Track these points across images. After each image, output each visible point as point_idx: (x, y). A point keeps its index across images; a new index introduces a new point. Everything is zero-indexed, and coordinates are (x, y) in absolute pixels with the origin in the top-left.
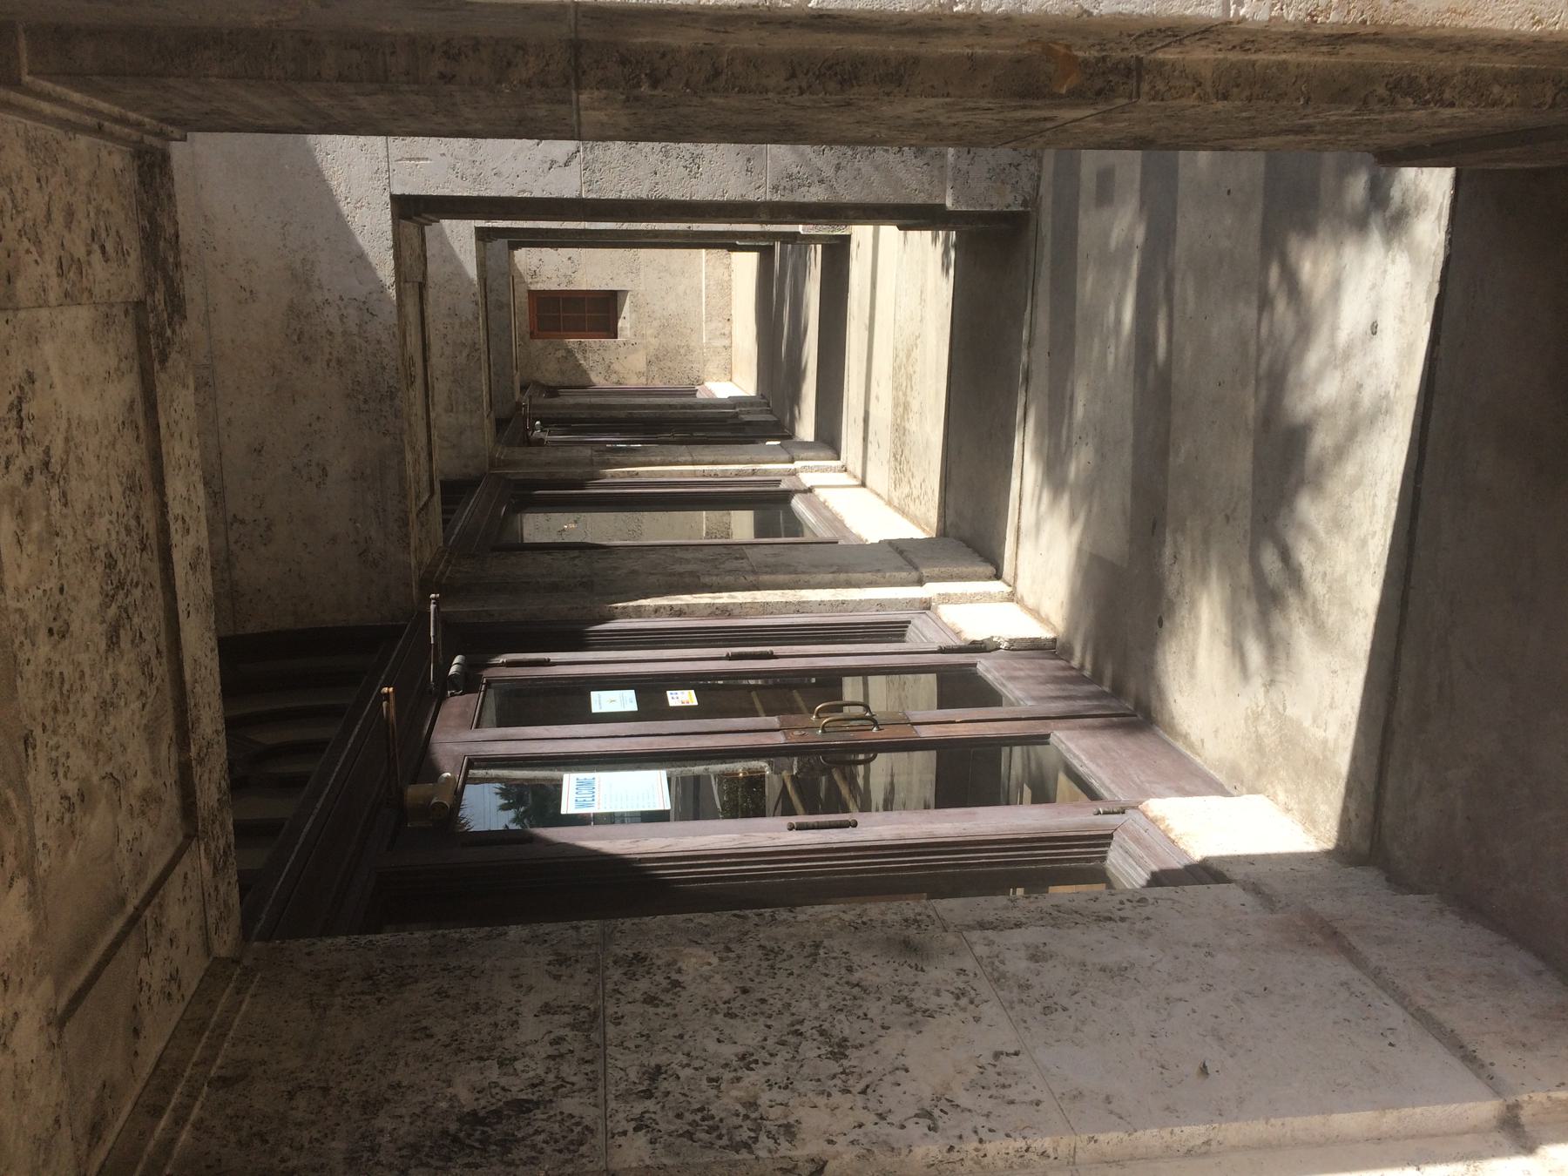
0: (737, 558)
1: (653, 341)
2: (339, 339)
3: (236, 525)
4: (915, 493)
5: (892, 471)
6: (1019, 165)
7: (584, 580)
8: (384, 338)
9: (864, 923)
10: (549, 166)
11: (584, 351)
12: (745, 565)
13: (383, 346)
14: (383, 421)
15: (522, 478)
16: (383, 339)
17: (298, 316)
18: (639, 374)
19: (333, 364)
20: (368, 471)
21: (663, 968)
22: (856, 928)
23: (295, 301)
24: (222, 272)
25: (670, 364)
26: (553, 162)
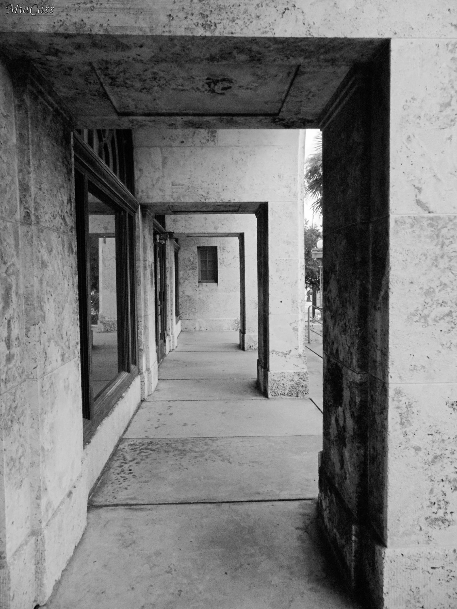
4: (126, 467)
5: (140, 441)
8: (263, 23)
10: (417, 186)
11: (193, 269)
12: (54, 364)
13: (254, 22)
18: (183, 292)
25: (188, 304)
26: (420, 190)
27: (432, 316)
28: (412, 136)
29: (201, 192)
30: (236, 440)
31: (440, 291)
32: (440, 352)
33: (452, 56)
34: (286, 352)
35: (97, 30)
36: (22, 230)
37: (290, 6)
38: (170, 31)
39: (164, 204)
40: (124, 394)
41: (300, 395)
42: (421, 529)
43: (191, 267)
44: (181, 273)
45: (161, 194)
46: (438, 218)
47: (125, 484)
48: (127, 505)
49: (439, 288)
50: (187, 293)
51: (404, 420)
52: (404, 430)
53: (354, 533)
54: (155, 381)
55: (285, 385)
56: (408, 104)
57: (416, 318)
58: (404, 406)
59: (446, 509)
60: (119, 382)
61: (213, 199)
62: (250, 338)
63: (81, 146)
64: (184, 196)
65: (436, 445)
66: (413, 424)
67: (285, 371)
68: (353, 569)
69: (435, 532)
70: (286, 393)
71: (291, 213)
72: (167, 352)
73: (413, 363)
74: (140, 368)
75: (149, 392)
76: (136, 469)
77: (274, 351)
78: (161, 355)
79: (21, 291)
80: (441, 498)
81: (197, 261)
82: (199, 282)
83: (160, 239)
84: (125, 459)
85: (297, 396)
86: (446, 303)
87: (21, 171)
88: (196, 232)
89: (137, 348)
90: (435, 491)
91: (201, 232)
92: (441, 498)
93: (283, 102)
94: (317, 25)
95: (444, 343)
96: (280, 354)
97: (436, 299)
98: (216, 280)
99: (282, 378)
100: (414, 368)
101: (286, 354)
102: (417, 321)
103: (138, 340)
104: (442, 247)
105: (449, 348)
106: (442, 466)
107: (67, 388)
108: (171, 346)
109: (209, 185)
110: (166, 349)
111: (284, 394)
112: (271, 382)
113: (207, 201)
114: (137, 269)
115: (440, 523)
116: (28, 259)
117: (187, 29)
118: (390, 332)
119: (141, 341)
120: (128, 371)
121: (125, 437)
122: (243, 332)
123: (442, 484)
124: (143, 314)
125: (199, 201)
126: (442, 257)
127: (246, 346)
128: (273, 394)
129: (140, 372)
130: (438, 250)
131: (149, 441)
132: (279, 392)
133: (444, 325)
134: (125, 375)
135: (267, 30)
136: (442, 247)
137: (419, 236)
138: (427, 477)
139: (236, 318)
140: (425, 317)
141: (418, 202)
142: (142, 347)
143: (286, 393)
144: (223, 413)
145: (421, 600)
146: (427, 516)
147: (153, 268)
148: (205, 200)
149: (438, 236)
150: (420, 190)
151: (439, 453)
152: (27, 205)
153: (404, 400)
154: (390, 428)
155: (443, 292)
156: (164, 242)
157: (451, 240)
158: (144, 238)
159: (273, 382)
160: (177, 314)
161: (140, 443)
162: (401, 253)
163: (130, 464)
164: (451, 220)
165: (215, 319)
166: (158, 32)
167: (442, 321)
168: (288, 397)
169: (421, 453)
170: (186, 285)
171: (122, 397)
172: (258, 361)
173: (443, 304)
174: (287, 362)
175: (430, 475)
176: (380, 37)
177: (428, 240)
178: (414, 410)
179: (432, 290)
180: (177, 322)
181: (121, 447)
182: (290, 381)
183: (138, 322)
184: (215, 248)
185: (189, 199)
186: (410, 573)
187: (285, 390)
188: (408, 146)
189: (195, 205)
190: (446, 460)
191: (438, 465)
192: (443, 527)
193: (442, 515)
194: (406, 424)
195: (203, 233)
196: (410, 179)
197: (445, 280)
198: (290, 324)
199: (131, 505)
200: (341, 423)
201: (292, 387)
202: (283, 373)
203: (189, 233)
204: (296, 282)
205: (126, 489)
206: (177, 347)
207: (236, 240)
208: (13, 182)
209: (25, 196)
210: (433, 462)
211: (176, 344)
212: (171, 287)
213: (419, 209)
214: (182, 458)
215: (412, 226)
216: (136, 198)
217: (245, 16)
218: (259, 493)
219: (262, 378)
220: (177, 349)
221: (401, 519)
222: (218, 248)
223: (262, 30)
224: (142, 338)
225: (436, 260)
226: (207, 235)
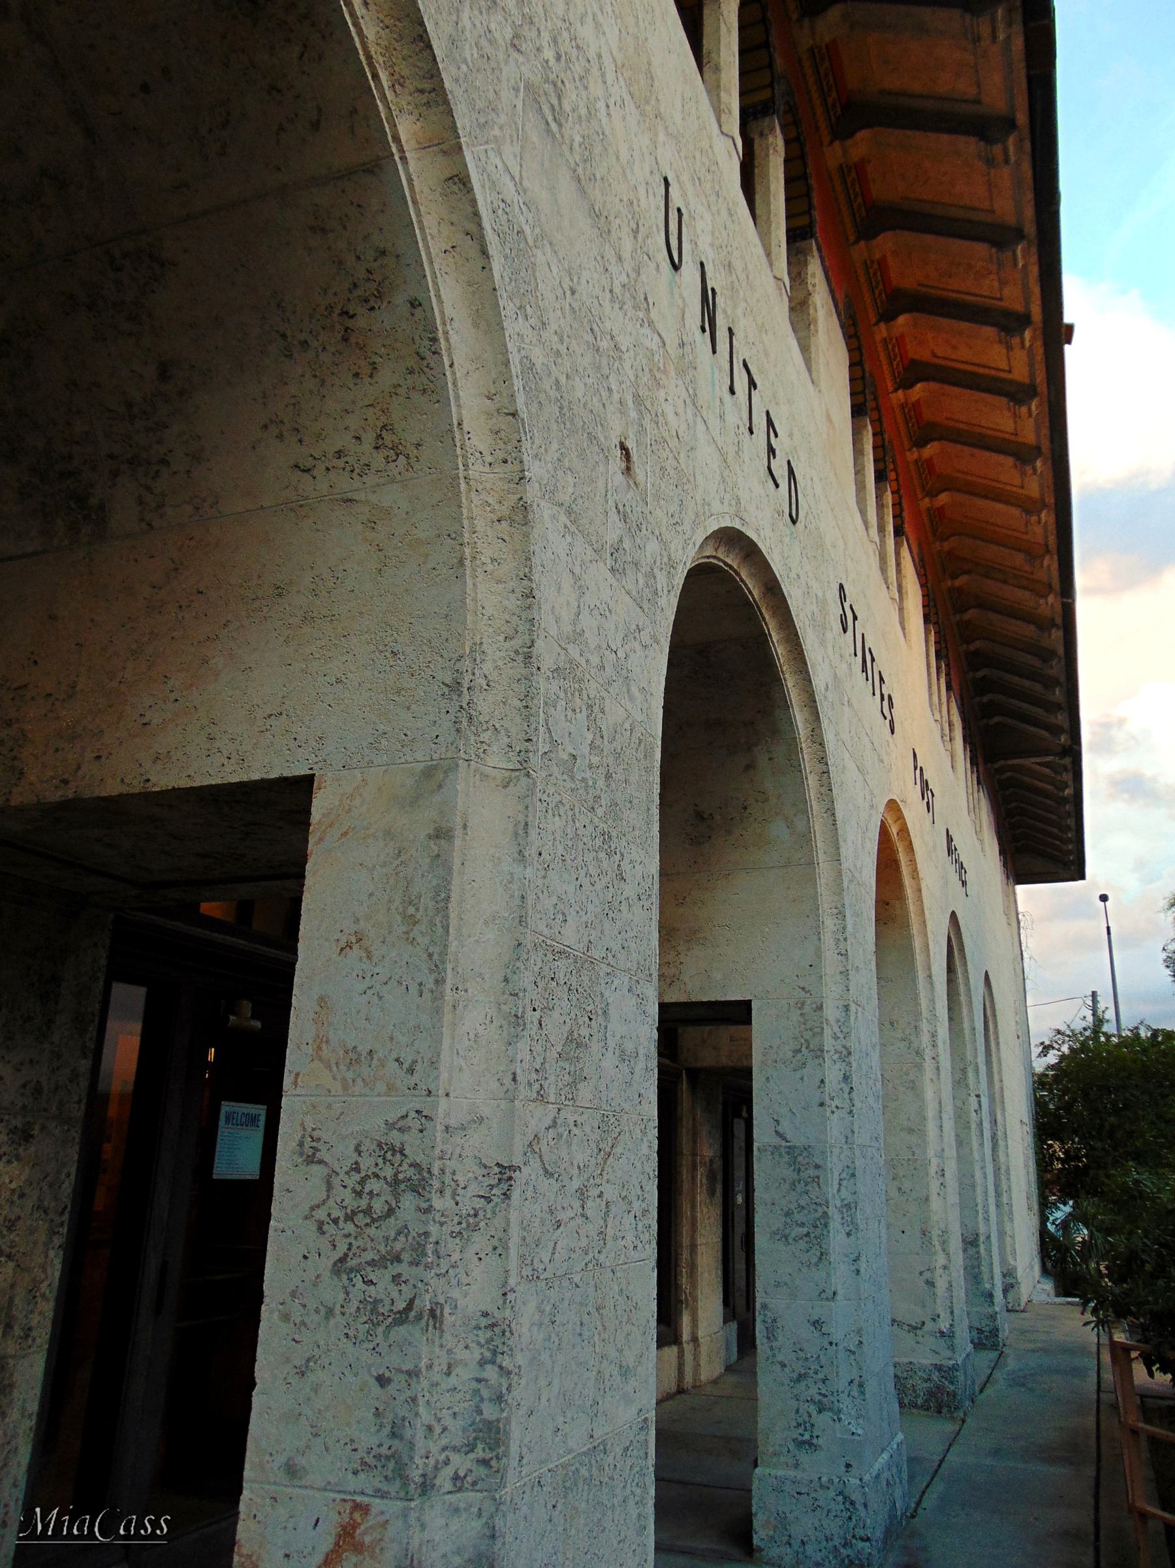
9: (35, 1297)
21: (15, 1152)
22: (31, 1291)
33: (800, 1012)
34: (914, 1324)
41: (945, 1410)
46: (795, 1147)
63: (998, 529)
65: (800, 1363)
67: (915, 1361)
80: (807, 1419)
89: (673, 1298)
92: (807, 1419)
96: (906, 1328)
101: (916, 1328)
104: (799, 1172)
111: (916, 1406)
123: (807, 1404)
126: (799, 1182)
130: (796, 1177)
133: (802, 1244)
136: (799, 1172)
140: (786, 1237)
145: (788, 1527)
151: (803, 1372)
155: (802, 1214)
168: (922, 1412)
169: (787, 1370)
174: (918, 1343)
191: (803, 1384)
197: (802, 1203)
198: (921, 1273)
202: (911, 1363)
204: (927, 1199)
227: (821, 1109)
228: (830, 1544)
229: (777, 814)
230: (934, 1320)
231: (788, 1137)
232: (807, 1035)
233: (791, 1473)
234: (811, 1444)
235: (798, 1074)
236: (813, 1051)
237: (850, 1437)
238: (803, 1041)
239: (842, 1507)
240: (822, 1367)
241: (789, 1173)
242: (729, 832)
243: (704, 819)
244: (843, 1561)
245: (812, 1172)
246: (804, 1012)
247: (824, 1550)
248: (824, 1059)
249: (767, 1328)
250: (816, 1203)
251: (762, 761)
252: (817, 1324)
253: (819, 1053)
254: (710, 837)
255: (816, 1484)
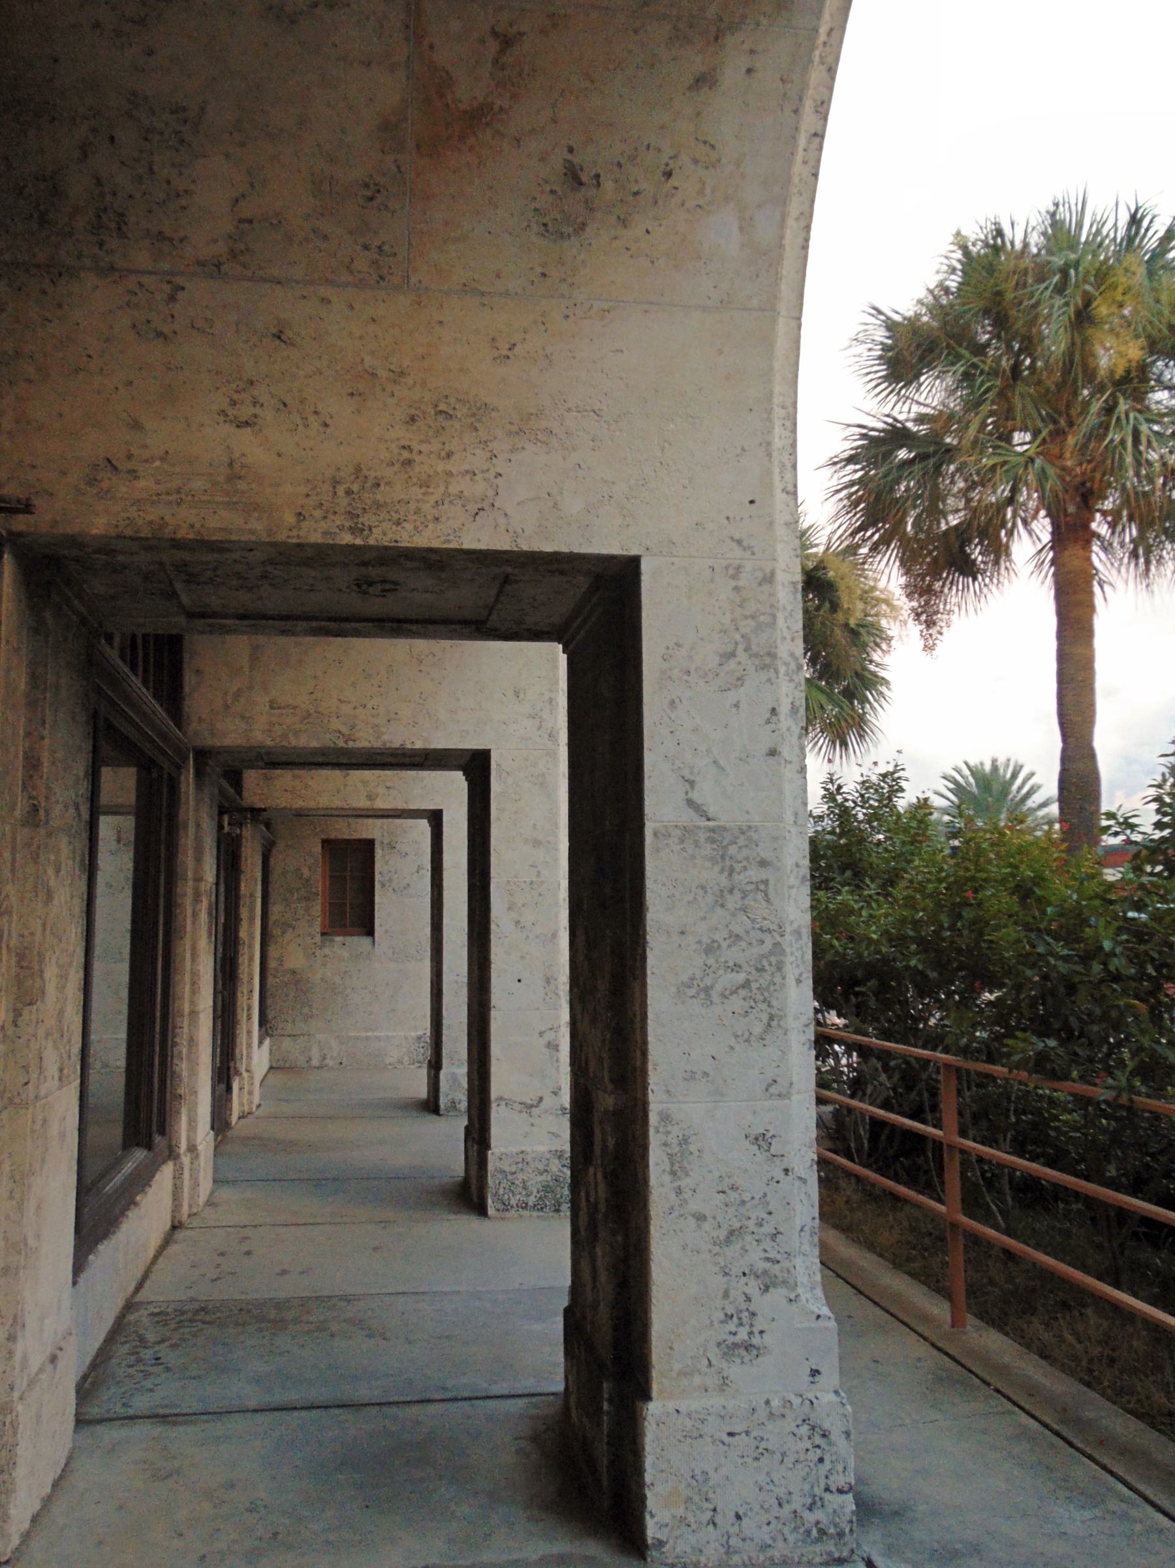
0: (61, 1070)
1: (319, 976)
2: (441, 467)
3: (167, 288)
4: (147, 1354)
6: (714, 1524)
7: (42, 813)
11: (307, 899)
13: (431, 526)
14: (318, 513)
15: (183, 790)
16: (440, 526)
17: (474, 415)
18: (281, 960)
19: (406, 454)
20: (241, 485)
23: (494, 414)
24: (535, 322)
25: (292, 995)
26: (692, 783)
27: (718, 987)
28: (677, 701)
29: (336, 724)
30: (402, 1299)
31: (730, 946)
32: (732, 1048)
33: (733, 583)
34: (529, 1102)
35: (183, 533)
36: (24, 834)
37: (485, 505)
38: (298, 536)
39: (250, 748)
40: (138, 1198)
42: (710, 1364)
43: (303, 892)
44: (276, 910)
45: (244, 726)
46: (724, 829)
47: (148, 1384)
48: (157, 1416)
49: (728, 942)
50: (290, 964)
51: (676, 1167)
52: (676, 1184)
53: (606, 1396)
54: (206, 1185)
55: (529, 1184)
56: (671, 652)
57: (693, 992)
58: (675, 1141)
59: (752, 1325)
60: (129, 1167)
61: (365, 740)
62: (454, 1078)
64: (297, 733)
65: (731, 1211)
66: (691, 1173)
67: (529, 1150)
68: (605, 1469)
69: (734, 1371)
70: (531, 1203)
71: (543, 775)
72: (234, 1118)
73: (688, 1068)
74: (174, 1143)
75: (190, 1206)
76: (171, 1358)
77: (501, 1098)
78: (220, 1122)
79: (14, 942)
81: (319, 877)
82: (323, 934)
83: (229, 824)
84: (142, 1339)
85: (558, 1211)
86: (740, 967)
87: (28, 734)
88: (321, 806)
89: (168, 1094)
90: (732, 1293)
91: (334, 806)
92: (743, 1306)
93: (492, 609)
94: (527, 533)
95: (739, 1033)
96: (517, 1107)
97: (722, 960)
98: (368, 930)
99: (520, 1165)
100: (691, 1076)
102: (693, 997)
103: (173, 1073)
104: (730, 875)
105: (747, 1041)
106: (742, 1248)
107: (62, 1135)
108: (245, 1101)
109: (355, 708)
110: (231, 1109)
111: (525, 1206)
112: (493, 1176)
113: (351, 744)
114: (179, 901)
115: (744, 1353)
116: (29, 886)
117: (325, 533)
118: (650, 1015)
119: (180, 1076)
120: (149, 1146)
121: (140, 1297)
122: (435, 1065)
123: (743, 1280)
124: (186, 1008)
125: (332, 745)
126: (731, 891)
127: (443, 1102)
128: (499, 1206)
129: (172, 1154)
130: (723, 880)
131: (196, 1305)
132: (513, 1202)
133: (737, 1003)
134: (139, 1155)
135: (451, 538)
136: (730, 875)
137: (693, 857)
138: (717, 1269)
139: (420, 1033)
140: (707, 990)
141: (690, 803)
142: (181, 1091)
143: (531, 1203)
144: (375, 1249)
145: (711, 1496)
146: (721, 1337)
147: (213, 898)
148: (346, 742)
149: (723, 857)
150: (692, 783)
151: (737, 1225)
152: (34, 793)
153: (675, 1131)
154: (653, 1181)
156: (238, 831)
157: (745, 863)
158: (198, 825)
159: (500, 1176)
160: (263, 1021)
161: (175, 1311)
162: (664, 885)
163: (157, 1349)
164: (743, 833)
165: (363, 1034)
166: (281, 537)
167: (735, 995)
168: (535, 1214)
169: (707, 1226)
170: (288, 944)
171: (136, 1204)
172: (467, 1128)
173: (737, 968)
174: (532, 1125)
175: (722, 1264)
176: (625, 553)
177: (708, 864)
178: (692, 1148)
179: (716, 945)
180: (261, 1043)
181: (131, 1318)
182: (541, 1174)
183: (175, 1027)
184: (369, 845)
185: (307, 741)
186: (691, 1445)
187: (528, 1195)
188: (673, 716)
189: (323, 751)
190: (748, 1238)
191: (736, 1247)
192: (747, 1359)
193: (746, 1337)
194: (679, 1173)
195: (336, 809)
196: (675, 767)
197: (739, 930)
198: (541, 1034)
199: (165, 1416)
200: (592, 1200)
201: (547, 1188)
202: (522, 1152)
203: (301, 809)
205: (151, 1390)
206: (259, 1106)
207: (423, 827)
208: (16, 756)
209: (31, 776)
210: (728, 1241)
211: (256, 1100)
212: (251, 947)
213: (691, 812)
214: (275, 1334)
215: (682, 841)
216: (185, 734)
217: (415, 517)
218: (444, 1389)
219: (474, 1168)
220: (260, 1112)
221: (675, 1346)
222: (377, 846)
223: (442, 539)
224: (183, 1067)
225: (722, 896)
226: (350, 813)
227: (771, 760)
228: (787, 1509)
229: (727, 199)
230: (555, 1093)
231: (712, 811)
232: (747, 626)
233: (715, 1401)
234: (748, 1347)
235: (732, 697)
236: (756, 655)
237: (814, 1324)
238: (738, 637)
239: (808, 1445)
240: (770, 1213)
241: (714, 876)
242: (624, 222)
243: (581, 184)
244: (808, 1532)
245: (754, 874)
246: (741, 583)
247: (774, 1522)
248: (777, 672)
249: (671, 1156)
250: (761, 929)
251: (731, 74)
252: (761, 1140)
253: (768, 660)
254: (583, 226)
255: (762, 1413)
